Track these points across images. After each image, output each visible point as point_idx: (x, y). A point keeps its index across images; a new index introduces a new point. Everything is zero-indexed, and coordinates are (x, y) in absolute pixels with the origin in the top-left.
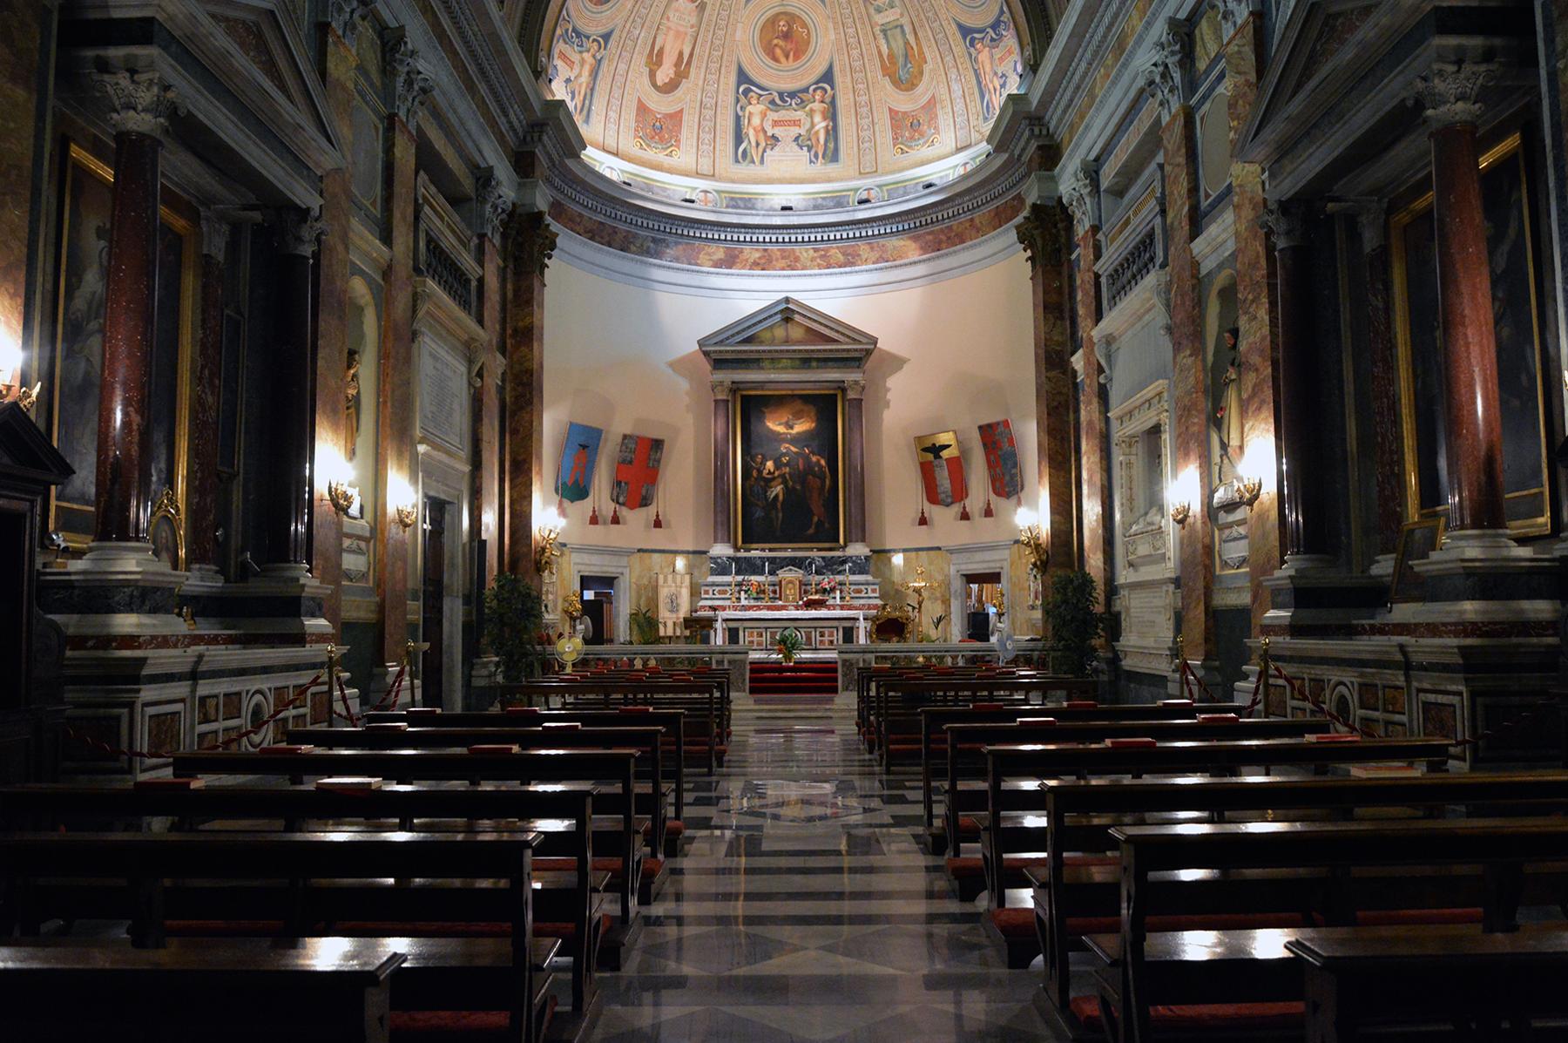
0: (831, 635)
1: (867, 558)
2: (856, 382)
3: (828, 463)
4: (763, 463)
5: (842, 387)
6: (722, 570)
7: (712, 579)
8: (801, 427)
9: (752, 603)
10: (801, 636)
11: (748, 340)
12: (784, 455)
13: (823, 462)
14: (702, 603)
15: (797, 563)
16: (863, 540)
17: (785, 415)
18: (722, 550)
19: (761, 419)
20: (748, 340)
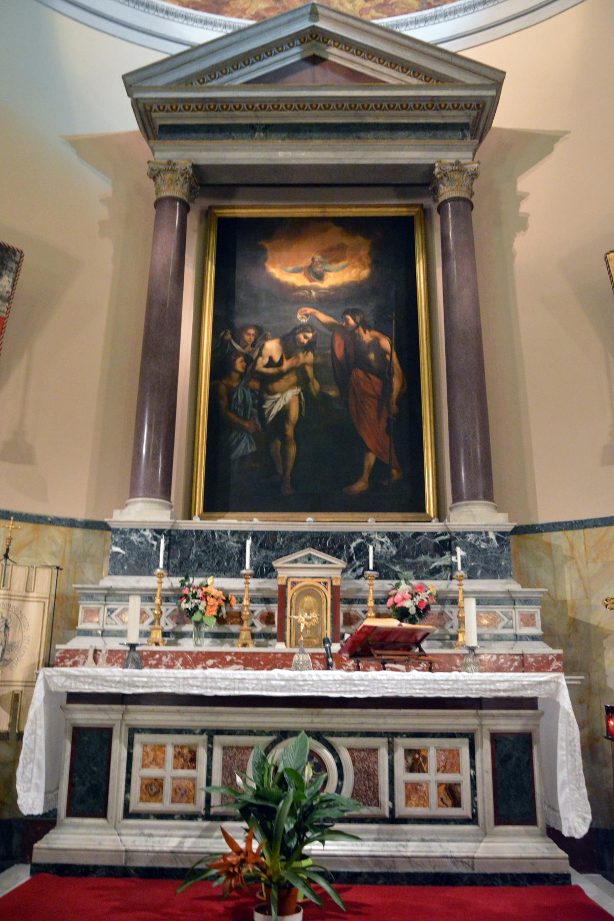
0: (450, 763)
1: (502, 537)
2: (458, 167)
3: (398, 346)
4: (258, 344)
5: (422, 181)
6: (138, 561)
7: (109, 582)
8: (342, 275)
9: (207, 645)
10: (339, 784)
11: (325, 562)
12: (303, 328)
13: (386, 343)
14: (77, 643)
15: (332, 544)
16: (488, 495)
17: (307, 254)
18: (145, 513)
19: (258, 259)
20: (325, 562)
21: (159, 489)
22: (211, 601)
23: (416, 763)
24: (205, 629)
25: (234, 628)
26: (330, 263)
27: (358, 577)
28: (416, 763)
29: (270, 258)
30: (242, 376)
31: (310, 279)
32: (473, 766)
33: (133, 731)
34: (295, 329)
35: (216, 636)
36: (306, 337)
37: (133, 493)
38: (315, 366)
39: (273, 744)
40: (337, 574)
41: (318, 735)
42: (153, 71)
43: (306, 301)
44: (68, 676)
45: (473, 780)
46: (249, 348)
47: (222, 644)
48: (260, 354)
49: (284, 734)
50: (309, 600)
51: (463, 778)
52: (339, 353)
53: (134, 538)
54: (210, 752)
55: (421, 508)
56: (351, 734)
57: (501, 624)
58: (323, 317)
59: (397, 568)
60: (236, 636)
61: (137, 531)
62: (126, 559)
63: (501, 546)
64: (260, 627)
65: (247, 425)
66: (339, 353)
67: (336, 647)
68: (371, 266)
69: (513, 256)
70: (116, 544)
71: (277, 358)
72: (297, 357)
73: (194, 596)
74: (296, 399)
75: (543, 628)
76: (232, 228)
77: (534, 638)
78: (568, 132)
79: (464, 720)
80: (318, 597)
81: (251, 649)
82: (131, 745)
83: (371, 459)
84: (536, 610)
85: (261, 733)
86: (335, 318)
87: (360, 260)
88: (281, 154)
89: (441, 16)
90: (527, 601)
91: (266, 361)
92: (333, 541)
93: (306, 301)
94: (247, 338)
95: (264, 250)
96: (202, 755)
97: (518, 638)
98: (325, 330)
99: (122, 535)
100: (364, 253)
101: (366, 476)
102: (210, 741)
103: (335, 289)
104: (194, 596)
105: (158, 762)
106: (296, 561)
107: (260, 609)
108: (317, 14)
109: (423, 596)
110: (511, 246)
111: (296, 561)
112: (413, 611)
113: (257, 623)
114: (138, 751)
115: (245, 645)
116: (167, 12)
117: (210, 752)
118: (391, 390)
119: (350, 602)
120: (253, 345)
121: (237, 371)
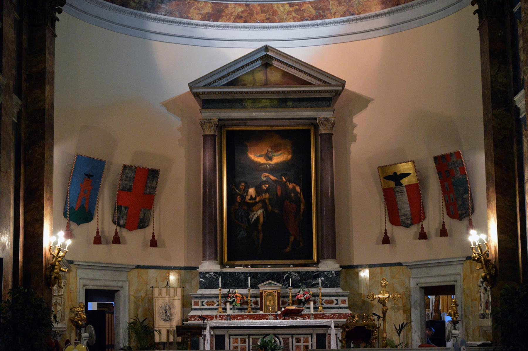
0: (306, 341)
1: (337, 273)
2: (327, 120)
4: (246, 190)
5: (314, 123)
7: (201, 292)
8: (278, 158)
9: (237, 313)
11: (275, 285)
12: (264, 182)
13: (298, 189)
18: (210, 266)
19: (245, 152)
20: (275, 285)
21: (213, 256)
22: (238, 298)
23: (298, 341)
24: (236, 307)
25: (245, 307)
26: (275, 152)
27: (287, 288)
28: (298, 341)
29: (249, 150)
30: (240, 204)
31: (266, 159)
32: (312, 341)
33: (230, 335)
34: (261, 183)
35: (238, 309)
36: (265, 187)
37: (204, 258)
38: (269, 199)
39: (264, 337)
40: (279, 288)
41: (275, 335)
42: (200, 80)
43: (265, 170)
44: (215, 323)
45: (312, 344)
46: (242, 192)
47: (241, 312)
48: (247, 195)
49: (267, 335)
50: (270, 297)
51: (309, 344)
52: (279, 193)
53: (207, 275)
54: (249, 340)
55: (312, 258)
56: (282, 335)
57: (335, 303)
58: (272, 177)
59: (300, 284)
60: (247, 309)
61: (208, 273)
62: (205, 283)
63: (336, 276)
64: (253, 306)
65: (242, 225)
66: (279, 193)
67: (279, 312)
68: (292, 153)
69: (350, 153)
70: (201, 278)
71: (254, 196)
72: (262, 196)
73: (233, 297)
74: (262, 214)
75: (348, 304)
76: (234, 141)
77: (345, 308)
78: (373, 100)
79: (310, 331)
80: (273, 297)
81: (252, 313)
82: (230, 339)
83: (292, 238)
84: (346, 298)
85: (261, 335)
86: (277, 178)
87: (288, 151)
88: (254, 114)
89: (324, 24)
90: (343, 296)
91: (249, 197)
92: (277, 275)
93: (265, 170)
94: (241, 187)
95: (247, 146)
96: (247, 340)
97: (340, 308)
98: (273, 183)
99: (203, 274)
100: (289, 147)
101: (290, 245)
102: (249, 337)
103: (277, 164)
104: (233, 297)
105: (237, 342)
106: (265, 285)
107: (253, 300)
108: (268, 49)
109: (307, 295)
110: (349, 148)
111: (265, 285)
112: (304, 300)
113: (252, 304)
114: (231, 340)
115: (249, 312)
116: (197, 25)
117: (249, 340)
118: (300, 209)
119: (284, 297)
120: (244, 190)
121: (238, 202)
